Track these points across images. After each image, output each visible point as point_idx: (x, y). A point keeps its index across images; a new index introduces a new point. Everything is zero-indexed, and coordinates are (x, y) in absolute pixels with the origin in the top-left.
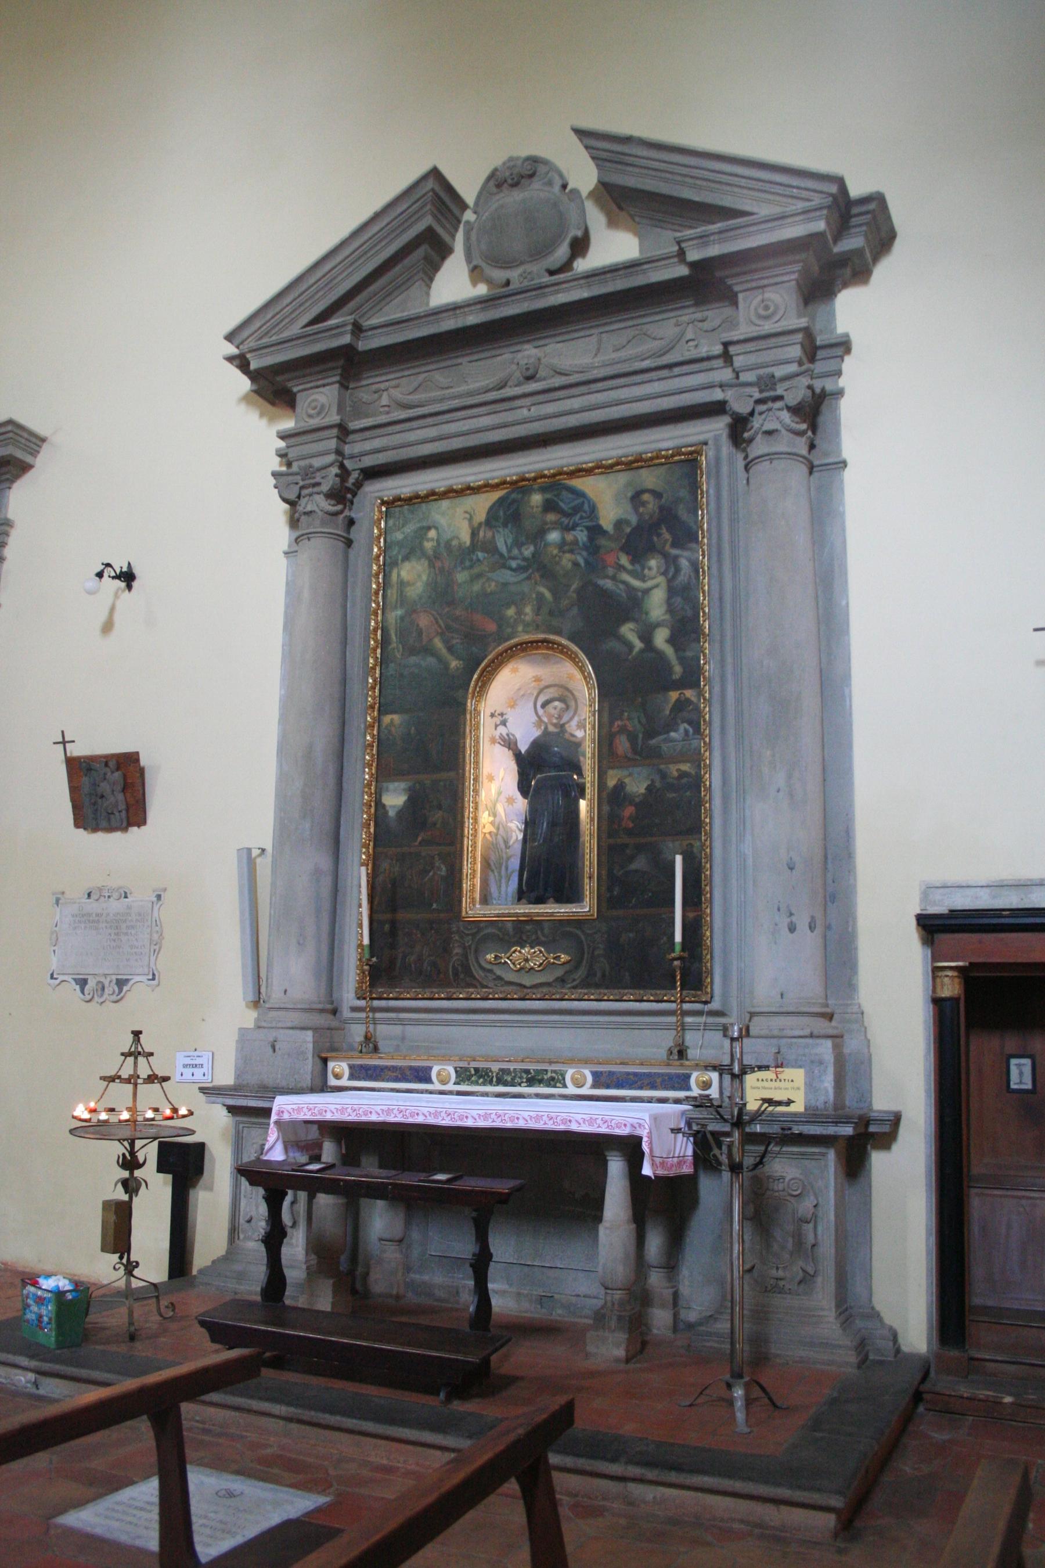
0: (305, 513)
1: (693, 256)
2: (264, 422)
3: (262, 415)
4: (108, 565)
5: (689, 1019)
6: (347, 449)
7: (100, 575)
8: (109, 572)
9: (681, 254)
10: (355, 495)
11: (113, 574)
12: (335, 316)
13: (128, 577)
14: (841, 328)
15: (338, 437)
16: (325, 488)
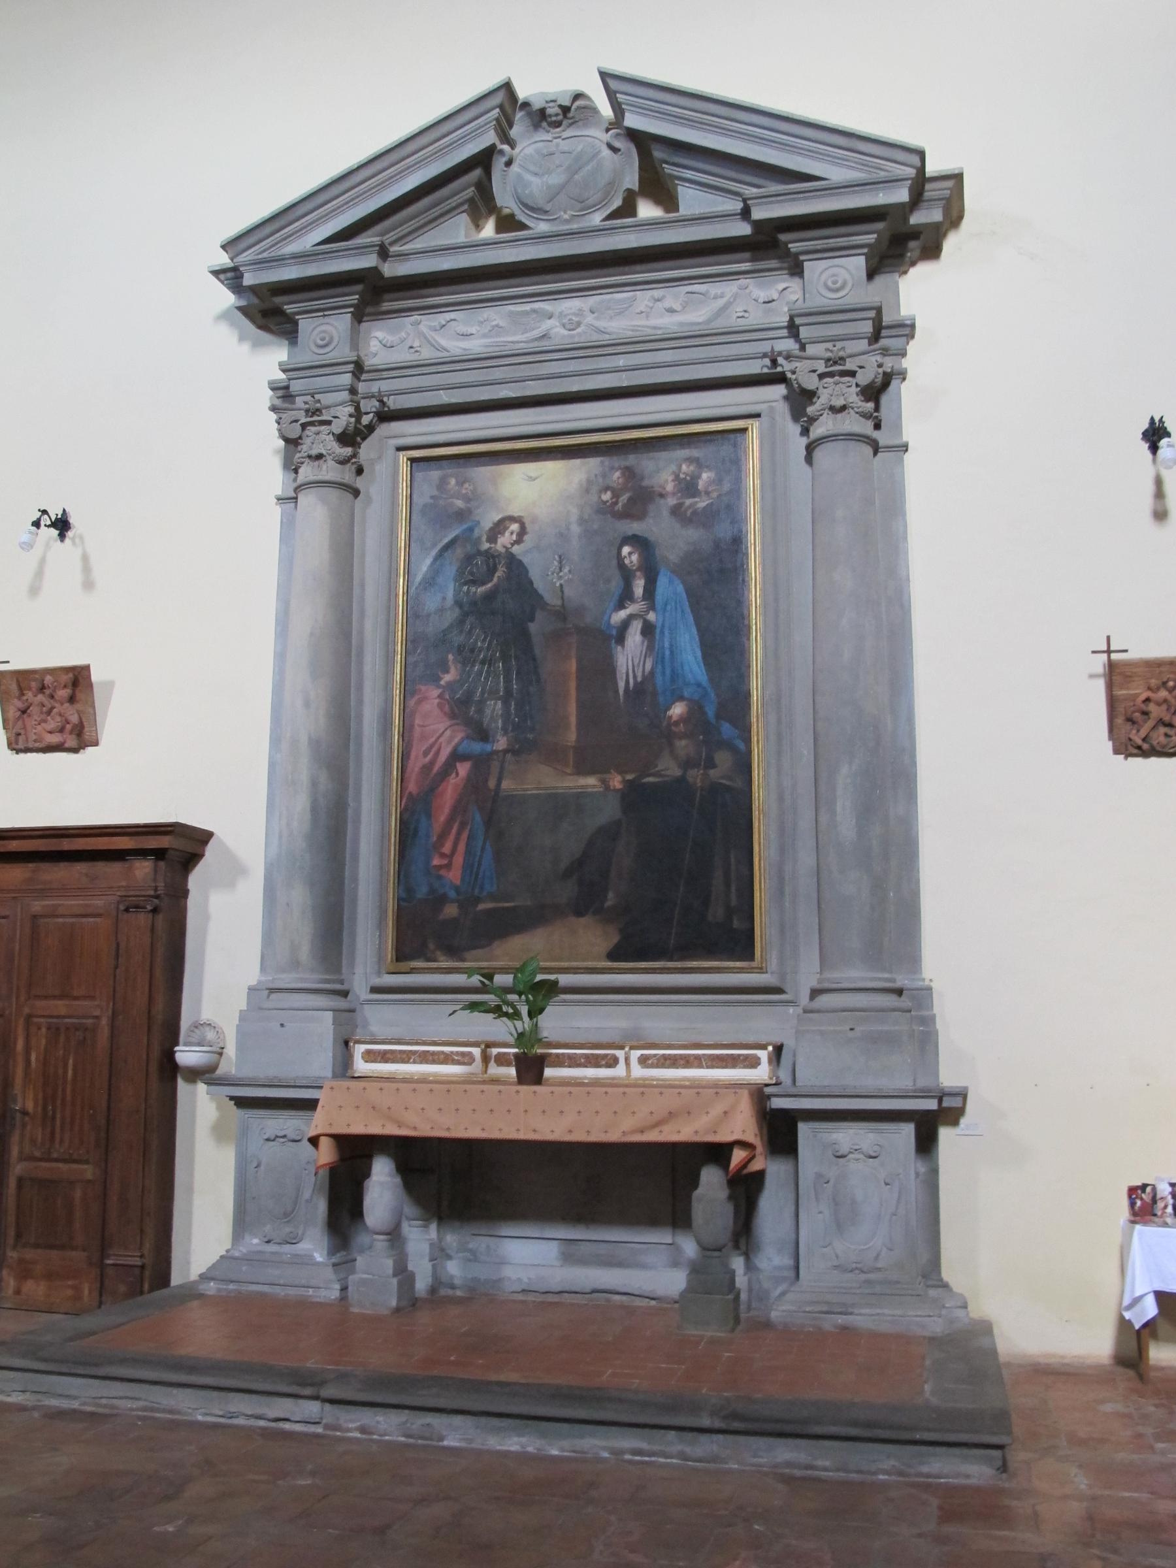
0: (310, 457)
1: (758, 214)
2: (246, 347)
3: (242, 339)
4: (44, 512)
5: (152, 893)
6: (362, 387)
7: (37, 524)
8: (45, 520)
9: (745, 213)
10: (364, 439)
11: (49, 523)
12: (364, 235)
13: (62, 525)
14: (905, 312)
15: (352, 372)
16: (338, 427)
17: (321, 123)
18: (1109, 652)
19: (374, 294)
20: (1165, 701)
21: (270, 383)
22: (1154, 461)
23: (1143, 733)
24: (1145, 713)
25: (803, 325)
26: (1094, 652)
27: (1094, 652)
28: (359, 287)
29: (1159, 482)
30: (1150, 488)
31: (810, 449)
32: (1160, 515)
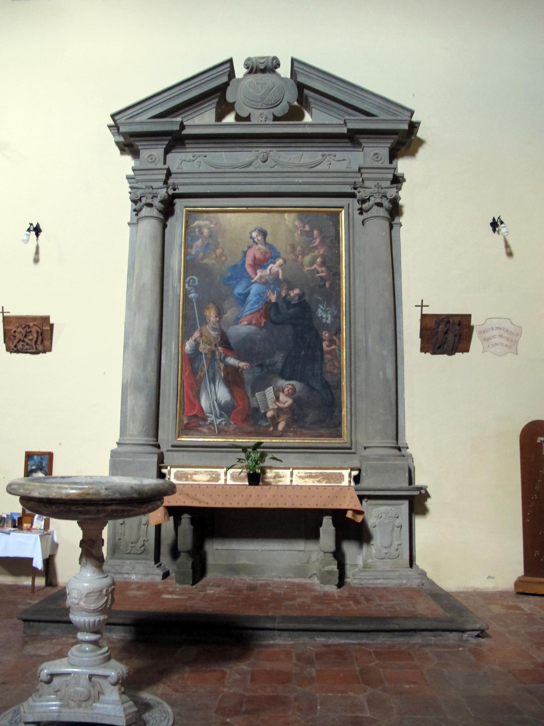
9: (345, 124)
17: (163, 60)
18: (422, 306)
19: (176, 140)
20: (21, 332)
21: (127, 176)
22: (37, 240)
23: (14, 344)
24: (15, 336)
25: (356, 172)
26: (416, 306)
27: (416, 306)
28: (170, 138)
29: (37, 248)
30: (34, 250)
31: (363, 223)
32: (36, 261)
